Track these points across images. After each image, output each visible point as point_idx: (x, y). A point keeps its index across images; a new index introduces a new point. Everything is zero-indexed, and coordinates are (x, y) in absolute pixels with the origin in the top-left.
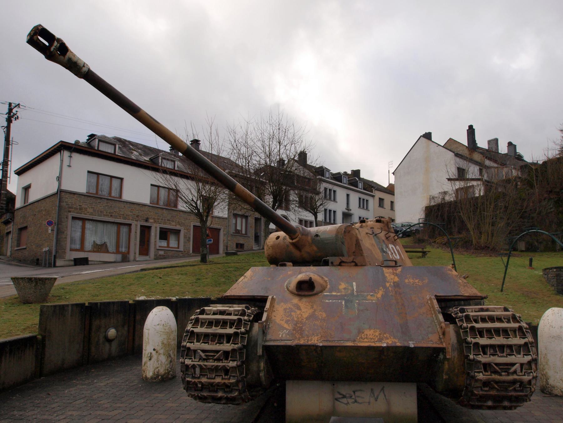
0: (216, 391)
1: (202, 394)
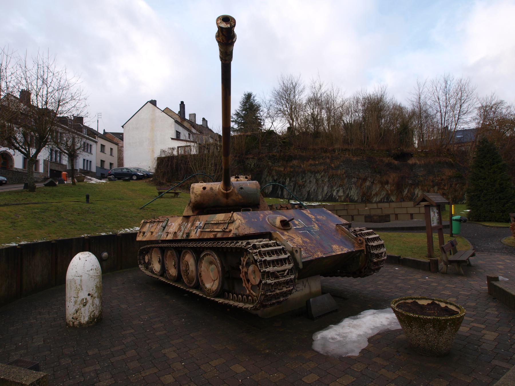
0: (279, 298)
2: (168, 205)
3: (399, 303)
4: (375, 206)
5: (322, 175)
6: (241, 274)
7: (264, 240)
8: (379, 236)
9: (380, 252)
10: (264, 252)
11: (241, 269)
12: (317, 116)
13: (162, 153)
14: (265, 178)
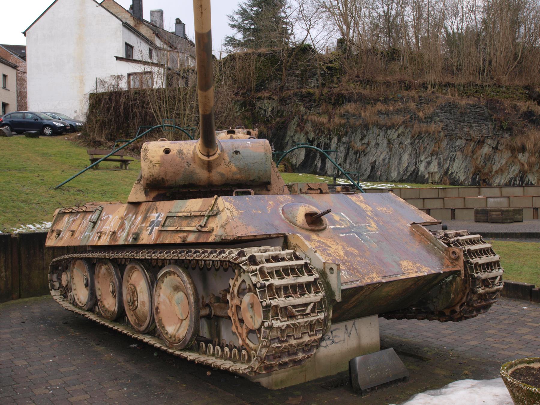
0: (295, 354)
1: (283, 360)
2: (108, 182)
3: (516, 368)
4: (496, 191)
5: (400, 132)
6: (229, 309)
7: (273, 248)
8: (491, 248)
9: (491, 275)
10: (269, 271)
11: (229, 300)
12: (395, 18)
13: (98, 86)
14: (292, 137)
